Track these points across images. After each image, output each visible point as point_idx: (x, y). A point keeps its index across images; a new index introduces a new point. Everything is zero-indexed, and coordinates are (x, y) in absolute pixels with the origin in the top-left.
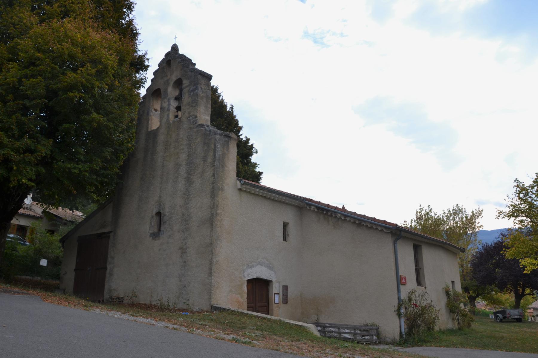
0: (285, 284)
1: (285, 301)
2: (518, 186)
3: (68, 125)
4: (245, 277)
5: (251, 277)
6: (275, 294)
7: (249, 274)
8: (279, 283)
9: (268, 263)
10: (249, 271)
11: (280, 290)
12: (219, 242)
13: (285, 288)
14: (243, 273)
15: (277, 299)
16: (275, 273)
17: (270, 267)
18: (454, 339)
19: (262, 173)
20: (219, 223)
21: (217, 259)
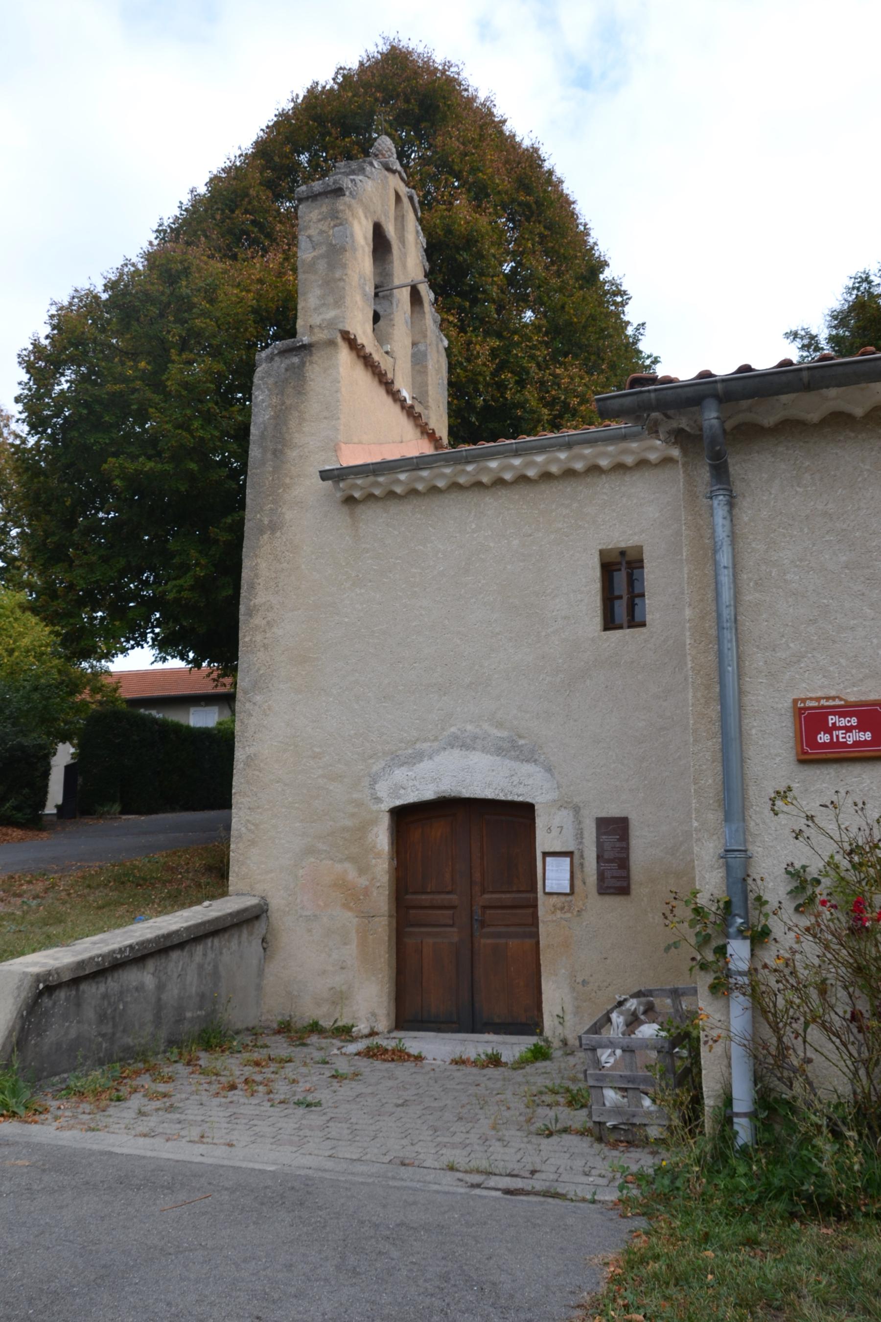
0: (613, 811)
1: (615, 878)
2: (27, 470)
3: (430, 388)
4: (378, 800)
5: (411, 797)
6: (546, 854)
7: (397, 788)
8: (577, 810)
9: (505, 734)
10: (400, 774)
11: (579, 835)
12: (258, 698)
13: (615, 831)
14: (372, 785)
15: (555, 876)
16: (549, 770)
17: (515, 749)
18: (800, 750)
19: (787, 335)
20: (258, 638)
21: (250, 751)
